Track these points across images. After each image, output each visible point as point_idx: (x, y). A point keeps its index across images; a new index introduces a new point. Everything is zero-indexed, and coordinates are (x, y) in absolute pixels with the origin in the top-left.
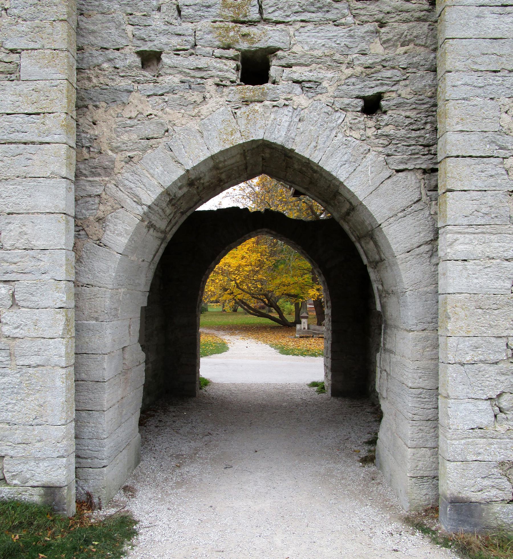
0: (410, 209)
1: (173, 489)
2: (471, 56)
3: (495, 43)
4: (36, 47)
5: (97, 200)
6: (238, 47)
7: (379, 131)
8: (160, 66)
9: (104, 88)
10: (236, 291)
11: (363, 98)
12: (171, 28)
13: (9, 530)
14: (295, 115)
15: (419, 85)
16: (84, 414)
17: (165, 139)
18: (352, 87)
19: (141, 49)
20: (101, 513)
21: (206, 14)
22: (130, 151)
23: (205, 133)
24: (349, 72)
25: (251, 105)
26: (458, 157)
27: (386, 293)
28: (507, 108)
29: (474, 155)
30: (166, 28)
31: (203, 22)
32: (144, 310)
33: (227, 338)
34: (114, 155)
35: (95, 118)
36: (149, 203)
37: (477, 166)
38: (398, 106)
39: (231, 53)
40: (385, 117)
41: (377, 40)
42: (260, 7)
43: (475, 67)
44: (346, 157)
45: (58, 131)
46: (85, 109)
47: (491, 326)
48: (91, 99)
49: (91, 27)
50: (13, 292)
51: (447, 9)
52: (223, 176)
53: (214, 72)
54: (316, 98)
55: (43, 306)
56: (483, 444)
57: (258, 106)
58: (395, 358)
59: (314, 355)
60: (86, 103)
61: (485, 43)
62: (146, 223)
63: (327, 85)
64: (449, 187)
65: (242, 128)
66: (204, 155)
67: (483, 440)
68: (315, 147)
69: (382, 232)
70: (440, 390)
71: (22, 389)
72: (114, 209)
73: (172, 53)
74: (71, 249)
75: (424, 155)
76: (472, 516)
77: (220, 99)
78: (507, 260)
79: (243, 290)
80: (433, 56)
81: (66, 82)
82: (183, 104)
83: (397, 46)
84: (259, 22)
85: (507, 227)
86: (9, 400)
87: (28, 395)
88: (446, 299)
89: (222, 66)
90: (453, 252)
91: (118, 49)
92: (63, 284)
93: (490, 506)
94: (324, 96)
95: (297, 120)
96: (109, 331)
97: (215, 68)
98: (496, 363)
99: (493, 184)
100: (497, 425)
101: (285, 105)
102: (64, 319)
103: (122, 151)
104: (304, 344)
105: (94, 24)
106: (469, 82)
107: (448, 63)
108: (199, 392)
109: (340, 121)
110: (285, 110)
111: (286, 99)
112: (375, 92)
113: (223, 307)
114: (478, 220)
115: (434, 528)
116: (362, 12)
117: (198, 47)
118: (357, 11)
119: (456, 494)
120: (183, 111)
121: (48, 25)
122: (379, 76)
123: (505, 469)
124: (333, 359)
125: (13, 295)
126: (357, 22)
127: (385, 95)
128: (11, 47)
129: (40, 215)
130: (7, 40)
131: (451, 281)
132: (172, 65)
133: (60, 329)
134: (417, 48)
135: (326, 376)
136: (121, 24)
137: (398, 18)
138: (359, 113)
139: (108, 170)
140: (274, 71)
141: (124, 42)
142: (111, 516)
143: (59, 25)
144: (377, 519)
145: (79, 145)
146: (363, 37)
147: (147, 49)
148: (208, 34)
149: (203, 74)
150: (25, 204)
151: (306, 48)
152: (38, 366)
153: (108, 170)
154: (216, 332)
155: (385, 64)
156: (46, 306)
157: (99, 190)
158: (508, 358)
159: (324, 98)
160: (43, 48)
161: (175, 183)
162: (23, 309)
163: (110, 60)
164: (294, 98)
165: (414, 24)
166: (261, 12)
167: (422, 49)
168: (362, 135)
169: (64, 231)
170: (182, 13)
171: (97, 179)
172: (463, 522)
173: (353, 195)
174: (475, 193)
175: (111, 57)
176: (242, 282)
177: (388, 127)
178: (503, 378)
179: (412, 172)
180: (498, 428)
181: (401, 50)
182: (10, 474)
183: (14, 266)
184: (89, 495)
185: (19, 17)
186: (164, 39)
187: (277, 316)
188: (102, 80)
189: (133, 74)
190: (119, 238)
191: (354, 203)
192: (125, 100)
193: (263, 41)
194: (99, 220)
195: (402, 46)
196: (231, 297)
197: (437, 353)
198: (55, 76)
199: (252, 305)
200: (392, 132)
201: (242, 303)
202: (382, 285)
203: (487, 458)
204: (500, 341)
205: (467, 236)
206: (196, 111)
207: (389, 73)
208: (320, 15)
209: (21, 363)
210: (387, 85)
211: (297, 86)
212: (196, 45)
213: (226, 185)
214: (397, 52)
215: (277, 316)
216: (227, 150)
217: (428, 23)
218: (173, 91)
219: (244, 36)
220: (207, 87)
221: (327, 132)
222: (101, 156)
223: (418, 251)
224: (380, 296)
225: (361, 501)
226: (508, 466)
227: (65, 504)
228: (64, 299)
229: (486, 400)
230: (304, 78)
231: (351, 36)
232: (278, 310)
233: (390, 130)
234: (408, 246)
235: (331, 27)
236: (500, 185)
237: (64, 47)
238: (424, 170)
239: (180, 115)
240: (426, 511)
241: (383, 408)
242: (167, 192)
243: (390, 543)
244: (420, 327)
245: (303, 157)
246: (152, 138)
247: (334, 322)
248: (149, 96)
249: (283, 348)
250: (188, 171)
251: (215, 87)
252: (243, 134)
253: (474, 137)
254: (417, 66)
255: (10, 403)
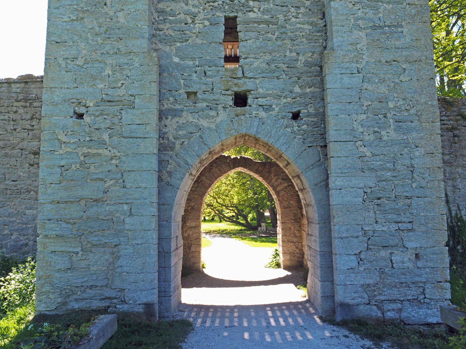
0: (315, 165)
11: (292, 113)
12: (201, 81)
23: (218, 131)
24: (285, 101)
26: (335, 141)
29: (342, 140)
40: (302, 122)
42: (243, 71)
44: (285, 141)
52: (224, 148)
57: (243, 117)
64: (332, 156)
71: (134, 255)
75: (321, 139)
78: (360, 188)
82: (208, 117)
83: (306, 88)
99: (351, 154)
112: (297, 110)
116: (290, 73)
118: (287, 73)
123: (365, 288)
128: (131, 94)
130: (129, 90)
140: (249, 101)
147: (190, 91)
148: (219, 84)
158: (363, 235)
164: (260, 113)
166: (243, 73)
170: (207, 74)
187: (243, 222)
195: (309, 88)
204: (358, 226)
208: (270, 74)
209: (134, 243)
210: (303, 106)
223: (320, 185)
230: (264, 104)
238: (321, 146)
246: (193, 133)
252: (236, 130)
255: (128, 263)
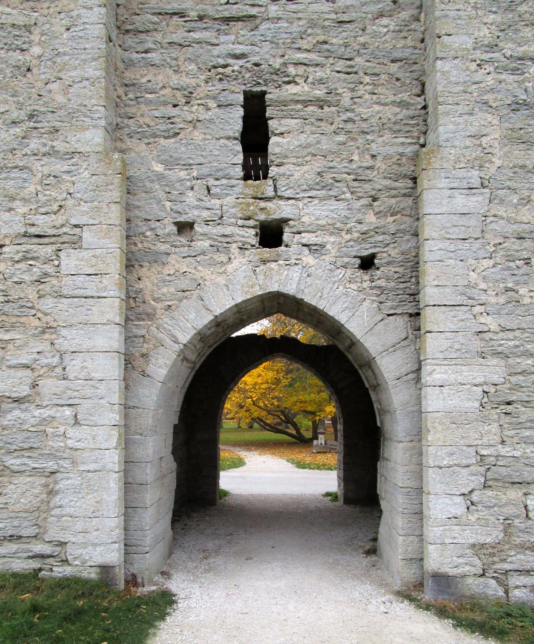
0: (399, 345)
1: (202, 574)
2: (444, 227)
3: (464, 218)
4: (95, 223)
5: (141, 340)
6: (257, 218)
7: (373, 284)
8: (193, 233)
9: (147, 252)
10: (253, 408)
11: (360, 257)
12: (202, 204)
13: (74, 598)
14: (304, 271)
15: (405, 247)
16: (130, 510)
17: (197, 291)
18: (350, 249)
19: (178, 220)
20: (145, 589)
21: (231, 192)
22: (168, 301)
23: (231, 287)
25: (268, 264)
26: (434, 305)
27: (384, 412)
28: (474, 267)
29: (448, 304)
30: (198, 203)
31: (228, 199)
32: (175, 426)
33: (243, 454)
34: (156, 304)
35: (140, 275)
36: (185, 342)
37: (450, 313)
38: (389, 263)
39: (251, 223)
40: (378, 272)
41: (371, 211)
42: (275, 186)
43: (448, 236)
45: (113, 288)
46: (132, 268)
47: (463, 437)
48: (137, 260)
49: (137, 203)
50: (76, 413)
51: (424, 191)
52: (244, 317)
53: (237, 238)
54: (321, 258)
55: (100, 424)
56: (458, 530)
57: (273, 265)
58: (391, 465)
59: (330, 469)
60: (132, 263)
61: (455, 218)
62: (181, 357)
63: (330, 248)
64: (428, 329)
65: (261, 282)
66: (229, 304)
67: (458, 527)
68: (321, 297)
69: (376, 363)
70: (425, 489)
72: (156, 347)
73: (203, 223)
74: (122, 379)
75: (410, 302)
76: (449, 587)
77: (242, 260)
78: (475, 385)
79: (259, 407)
80: (416, 223)
81: (119, 250)
82: (213, 264)
83: (387, 216)
84: (274, 198)
85: (475, 360)
86: (72, 498)
87: (88, 494)
88: (427, 416)
89: (243, 233)
90: (431, 380)
91: (159, 221)
92: (116, 407)
93: (465, 579)
94: (328, 256)
95: (305, 275)
96: (151, 444)
97: (238, 235)
98: (468, 466)
100: (469, 515)
101: (295, 264)
102: (117, 434)
103: (162, 301)
104: (321, 459)
105: (139, 201)
106: (443, 248)
107: (426, 233)
108: (219, 501)
109: (341, 276)
110: (296, 268)
111: (297, 259)
112: (370, 253)
113: (239, 424)
114: (452, 354)
115: (419, 598)
116: (358, 190)
117: (225, 218)
118: (354, 189)
119: (436, 570)
120: (212, 269)
121: (104, 206)
122: (372, 240)
124: (345, 470)
125: (76, 416)
126: (354, 198)
127: (378, 255)
128: (75, 223)
129: (98, 353)
130: (71, 217)
131: (430, 402)
132: (203, 233)
133: (114, 442)
134: (404, 218)
135: (339, 486)
136: (161, 201)
137: (387, 194)
138: (357, 270)
139: (151, 316)
140: (286, 237)
141: (164, 215)
142: (153, 591)
143: (113, 207)
144: (373, 593)
145: (128, 297)
146: (359, 210)
147: (182, 220)
148: (232, 208)
149: (228, 240)
150: (86, 344)
151: (313, 218)
152: (96, 471)
153: (151, 316)
154: (232, 448)
155: (377, 230)
156: (103, 424)
157: (143, 332)
158: (477, 462)
159: (327, 258)
160: (100, 223)
161: (206, 326)
162: (84, 427)
163: (152, 229)
164: (303, 259)
165: (401, 198)
167: (408, 218)
168: (359, 287)
169: (117, 366)
170: (211, 192)
171: (141, 323)
172: (442, 592)
173: (352, 334)
174: (449, 334)
175: (153, 226)
176: (259, 399)
177: (380, 280)
178: (473, 478)
179: (400, 316)
180: (470, 517)
181: (390, 219)
182: (72, 557)
183: (76, 393)
184: (134, 576)
185: (81, 200)
186: (196, 212)
187: (294, 432)
188: (145, 244)
189: (171, 240)
190: (160, 370)
191: (354, 340)
192: (164, 260)
193: (277, 213)
194: (143, 355)
195: (391, 216)
196: (247, 414)
197: (421, 460)
198: (110, 246)
199: (268, 421)
200: (383, 284)
201: (259, 420)
202: (380, 405)
203: (461, 541)
205: (443, 367)
206: (223, 269)
207: (380, 238)
208: (324, 192)
209: (82, 469)
211: (305, 248)
212: (222, 217)
213: (247, 323)
214: (388, 221)
215: (294, 432)
216: (248, 300)
217: (412, 198)
218: (204, 253)
219: (262, 209)
220: (232, 250)
221: (330, 285)
222: (145, 305)
223: (405, 378)
224: (379, 414)
225: (362, 582)
226: (479, 548)
227: (117, 580)
228: (118, 419)
229: (460, 495)
230: (311, 242)
231: (349, 209)
232: (295, 425)
233: (382, 283)
234: (398, 374)
235: (333, 202)
236: (469, 327)
237: (117, 223)
239: (210, 272)
240: (414, 586)
241: (382, 507)
242: (199, 333)
243: (382, 608)
244: (408, 439)
245: (311, 305)
246: (187, 291)
247: (345, 437)
248: (184, 257)
249: (299, 462)
250: (216, 316)
251: (238, 250)
252: (262, 287)
253: (447, 290)
254: (404, 232)
255: (72, 501)
